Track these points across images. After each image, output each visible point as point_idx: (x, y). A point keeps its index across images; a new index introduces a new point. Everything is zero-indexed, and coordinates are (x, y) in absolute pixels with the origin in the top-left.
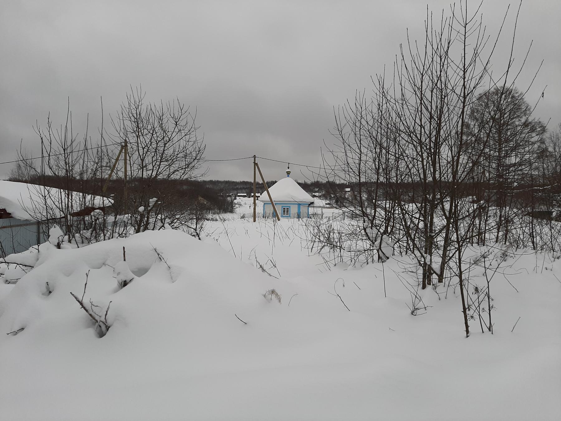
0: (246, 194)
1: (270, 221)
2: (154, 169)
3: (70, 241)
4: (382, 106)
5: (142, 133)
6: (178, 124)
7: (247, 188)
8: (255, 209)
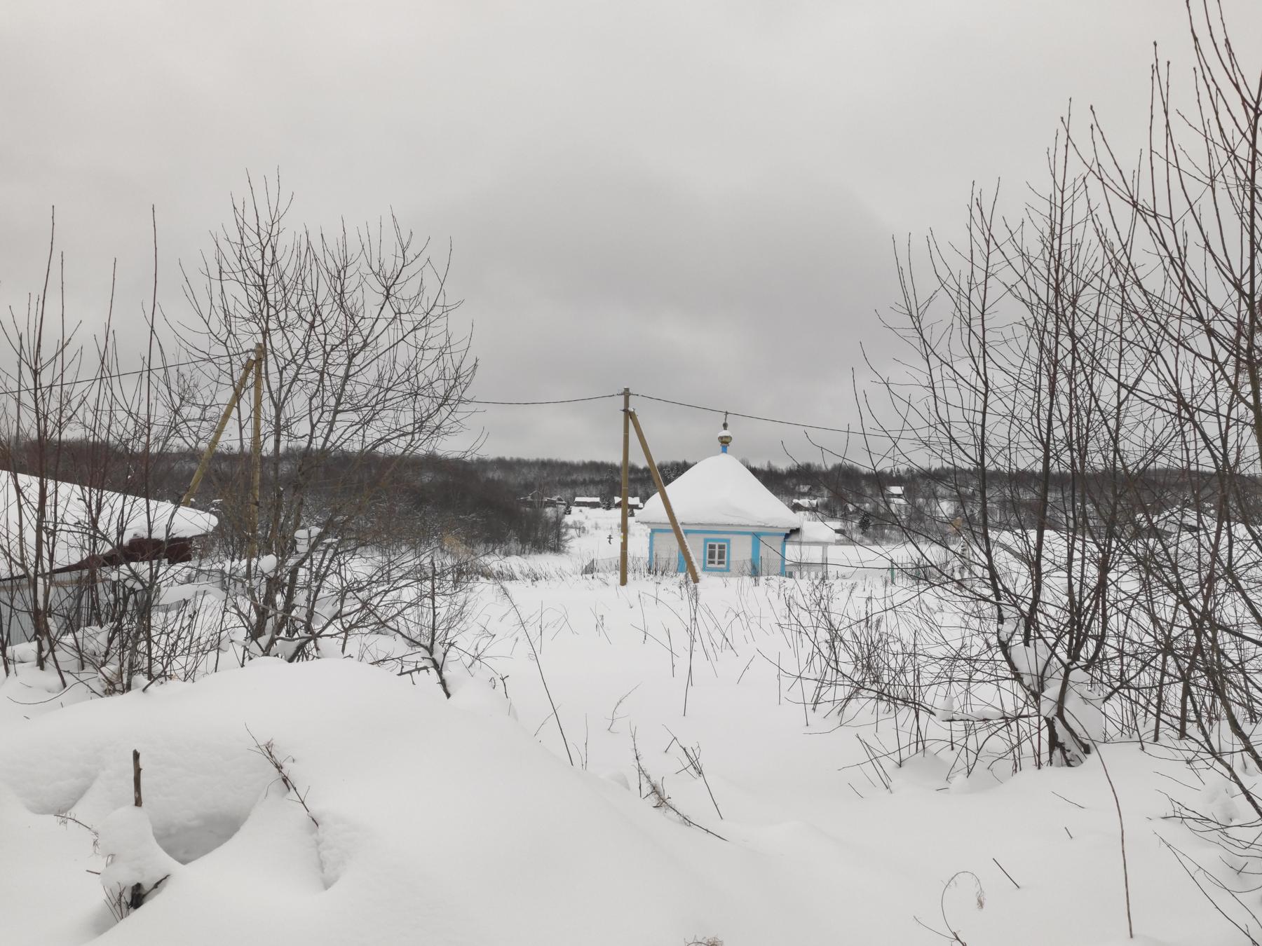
0: (597, 500)
1: (671, 586)
2: (318, 433)
3: (41, 663)
4: (1061, 234)
5: (280, 322)
6: (392, 292)
7: (601, 482)
8: (624, 546)
